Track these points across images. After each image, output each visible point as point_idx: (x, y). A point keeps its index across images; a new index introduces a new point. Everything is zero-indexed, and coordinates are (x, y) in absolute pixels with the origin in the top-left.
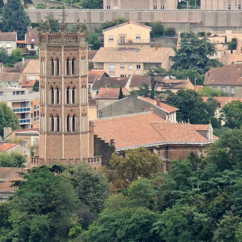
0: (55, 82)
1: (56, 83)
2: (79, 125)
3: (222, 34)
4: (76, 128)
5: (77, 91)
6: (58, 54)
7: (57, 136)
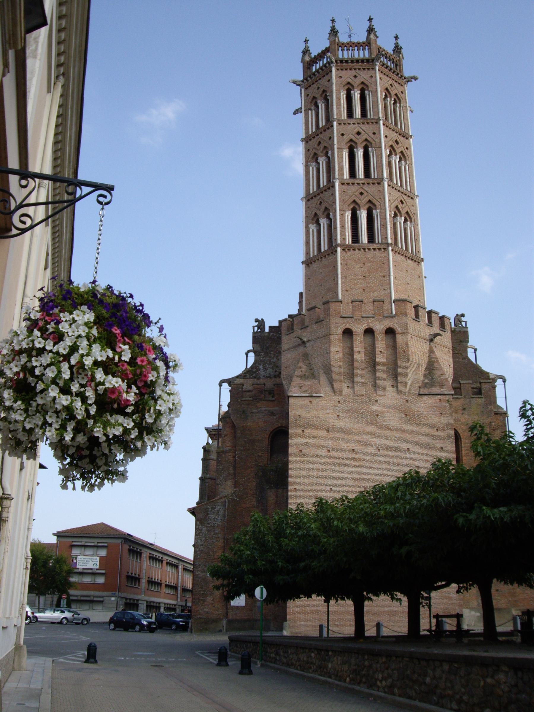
0: (361, 131)
1: (363, 133)
2: (417, 240)
3: (87, 592)
4: (400, 118)
5: (407, 167)
6: (364, 76)
7: (371, 254)
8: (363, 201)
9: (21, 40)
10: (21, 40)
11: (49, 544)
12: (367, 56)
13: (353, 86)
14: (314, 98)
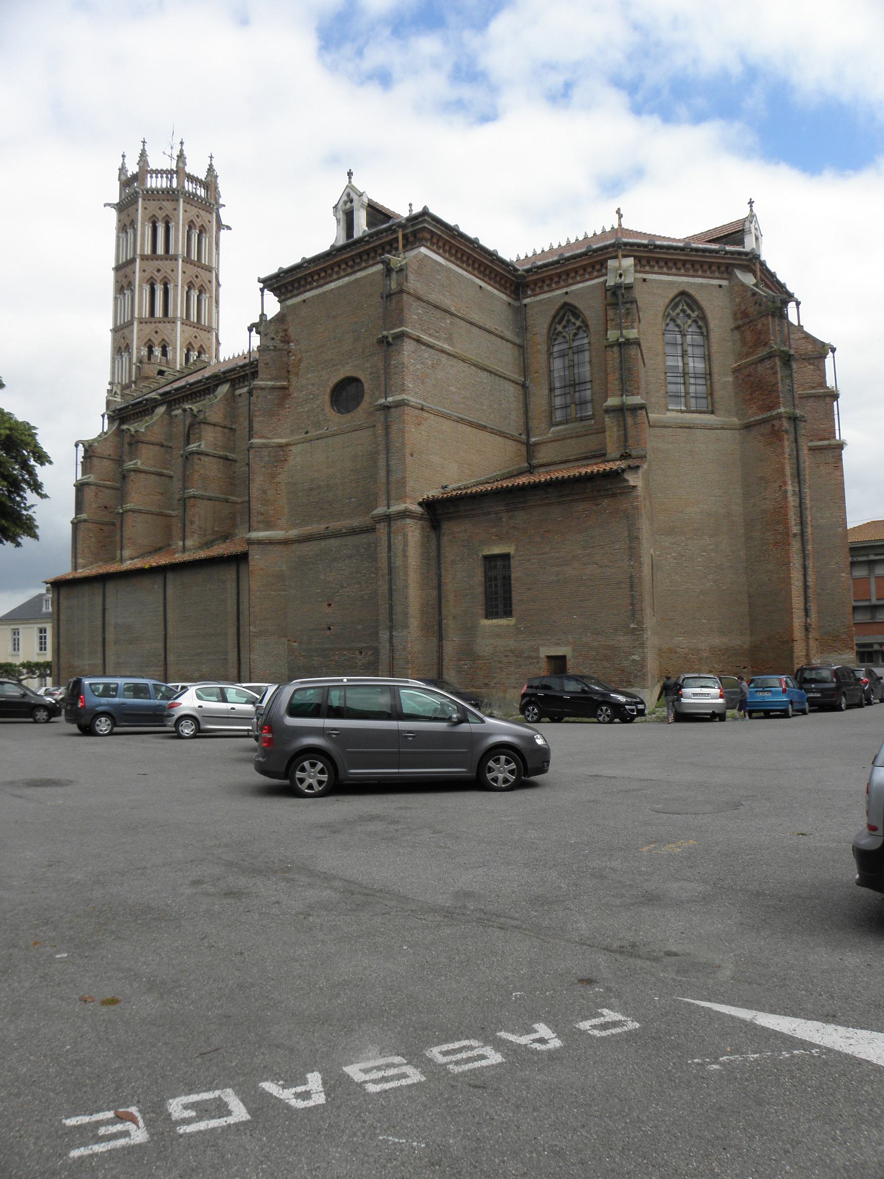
8: (156, 340)
9: (378, 1068)
10: (378, 1068)
11: (363, 711)
12: (175, 185)
13: (158, 219)
14: (125, 225)
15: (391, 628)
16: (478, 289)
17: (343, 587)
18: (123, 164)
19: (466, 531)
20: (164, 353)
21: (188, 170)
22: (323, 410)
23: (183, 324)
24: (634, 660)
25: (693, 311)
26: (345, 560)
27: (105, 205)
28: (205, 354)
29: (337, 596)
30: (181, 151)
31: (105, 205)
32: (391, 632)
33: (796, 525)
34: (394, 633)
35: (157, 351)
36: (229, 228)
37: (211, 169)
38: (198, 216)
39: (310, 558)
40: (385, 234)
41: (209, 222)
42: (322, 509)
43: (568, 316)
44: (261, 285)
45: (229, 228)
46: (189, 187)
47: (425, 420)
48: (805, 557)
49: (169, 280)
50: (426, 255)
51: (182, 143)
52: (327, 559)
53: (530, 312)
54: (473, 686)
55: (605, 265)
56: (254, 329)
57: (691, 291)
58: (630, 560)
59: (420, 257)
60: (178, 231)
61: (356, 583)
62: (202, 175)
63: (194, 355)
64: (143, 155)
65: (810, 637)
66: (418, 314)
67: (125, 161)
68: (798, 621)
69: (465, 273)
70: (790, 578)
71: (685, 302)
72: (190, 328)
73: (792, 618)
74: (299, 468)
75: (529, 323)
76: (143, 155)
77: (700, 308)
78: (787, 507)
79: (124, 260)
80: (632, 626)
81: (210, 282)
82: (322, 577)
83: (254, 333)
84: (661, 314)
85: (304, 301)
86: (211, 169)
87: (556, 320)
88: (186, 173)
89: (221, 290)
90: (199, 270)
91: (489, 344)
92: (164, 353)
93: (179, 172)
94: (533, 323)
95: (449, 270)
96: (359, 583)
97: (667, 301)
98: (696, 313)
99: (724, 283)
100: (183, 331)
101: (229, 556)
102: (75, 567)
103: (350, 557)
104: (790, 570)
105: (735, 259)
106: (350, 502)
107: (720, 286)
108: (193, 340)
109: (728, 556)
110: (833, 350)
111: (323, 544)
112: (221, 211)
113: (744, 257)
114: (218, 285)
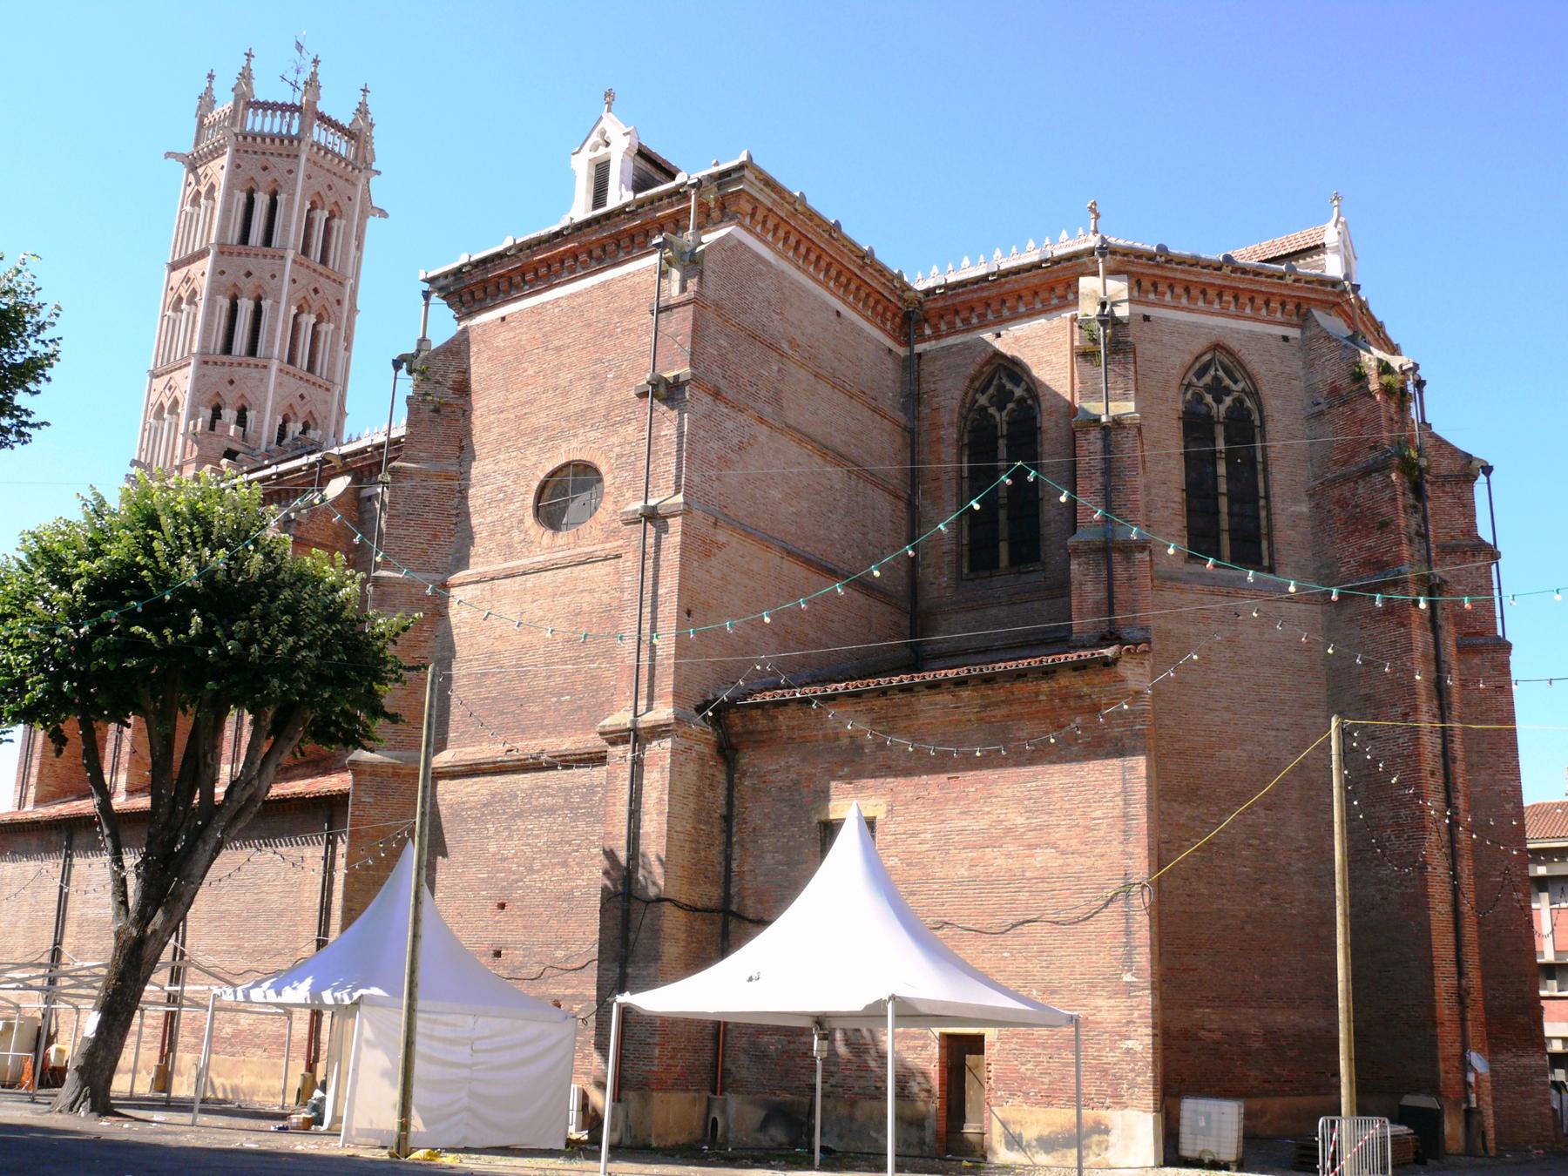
8: (230, 396)
15: (1126, 816)
16: (833, 317)
17: (530, 870)
18: (209, 89)
19: (788, 768)
20: (241, 420)
21: (321, 107)
22: (521, 521)
23: (281, 370)
24: (1128, 1051)
25: (1236, 382)
26: (540, 817)
27: (168, 155)
28: (315, 429)
29: (520, 888)
30: (314, 74)
31: (168, 155)
32: (623, 967)
33: (1436, 791)
34: (629, 970)
35: (229, 415)
36: (383, 213)
37: (363, 110)
38: (330, 187)
39: (471, 809)
40: (665, 201)
41: (350, 199)
42: (502, 713)
43: (1000, 378)
44: (426, 287)
45: (383, 213)
46: (319, 134)
47: (721, 546)
48: (1454, 857)
49: (265, 293)
50: (740, 243)
51: (316, 62)
52: (504, 813)
53: (927, 368)
54: (784, 1089)
55: (1073, 289)
56: (405, 365)
57: (1234, 345)
58: (1125, 841)
59: (731, 243)
60: (292, 208)
61: (559, 863)
62: (345, 119)
63: (295, 428)
64: (246, 76)
65: (1469, 1016)
66: (720, 347)
67: (214, 85)
68: (1444, 982)
69: (810, 284)
70: (1426, 896)
71: (1220, 363)
72: (293, 380)
73: (1432, 979)
74: (466, 630)
75: (924, 387)
76: (246, 76)
77: (1249, 376)
78: (1419, 755)
79: (190, 252)
80: (1127, 978)
81: (339, 302)
82: (492, 848)
83: (403, 372)
84: (1175, 383)
85: (503, 319)
86: (363, 110)
87: (977, 384)
88: (317, 113)
89: (359, 319)
90: (322, 279)
91: (849, 419)
92: (241, 420)
93: (309, 112)
94: (932, 387)
95: (780, 274)
96: (564, 864)
97: (1188, 359)
98: (1241, 385)
99: (1294, 333)
100: (280, 384)
101: (315, 798)
102: (22, 803)
103: (552, 811)
104: (1426, 880)
105: (1313, 290)
106: (561, 703)
107: (1286, 339)
108: (297, 402)
109: (1302, 848)
110: (1488, 470)
111: (499, 781)
112: (374, 180)
113: (1329, 289)
114: (353, 310)
